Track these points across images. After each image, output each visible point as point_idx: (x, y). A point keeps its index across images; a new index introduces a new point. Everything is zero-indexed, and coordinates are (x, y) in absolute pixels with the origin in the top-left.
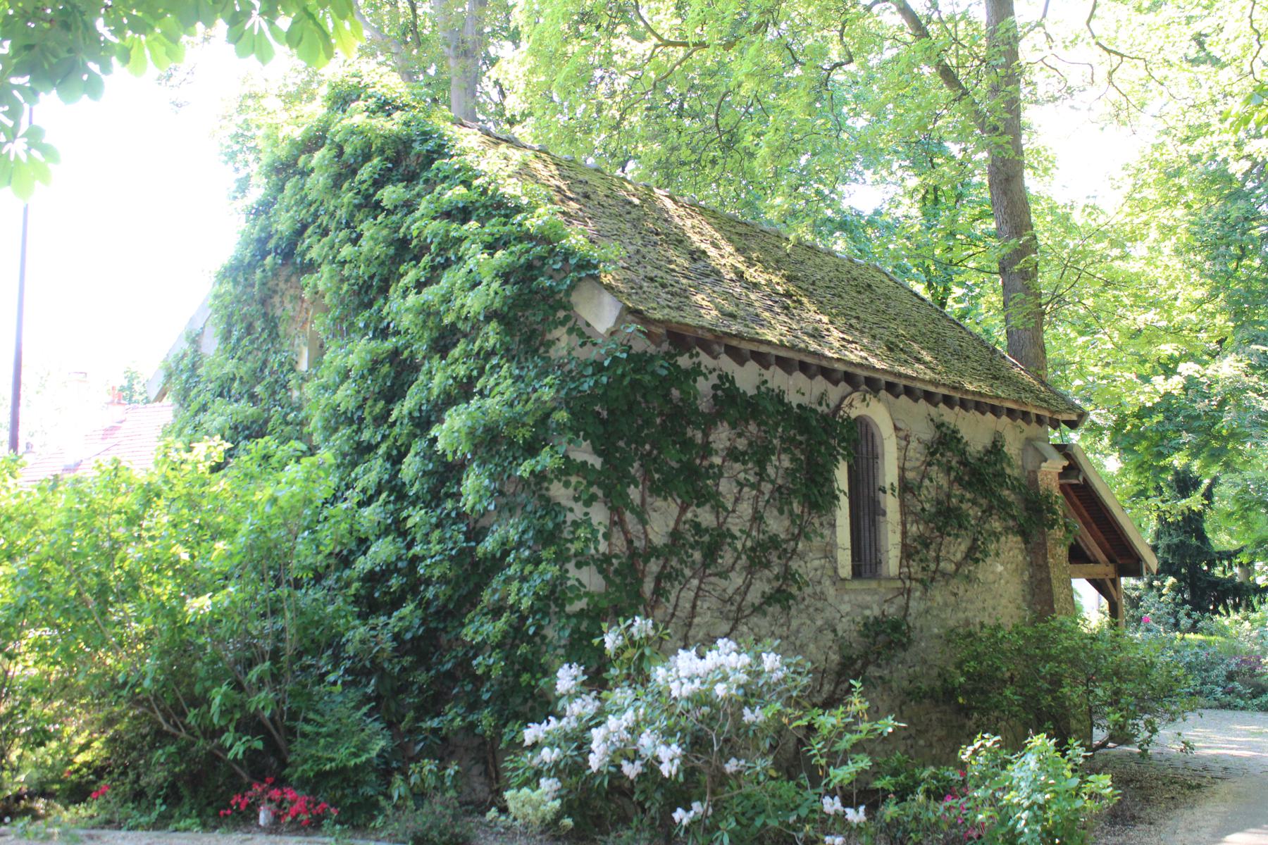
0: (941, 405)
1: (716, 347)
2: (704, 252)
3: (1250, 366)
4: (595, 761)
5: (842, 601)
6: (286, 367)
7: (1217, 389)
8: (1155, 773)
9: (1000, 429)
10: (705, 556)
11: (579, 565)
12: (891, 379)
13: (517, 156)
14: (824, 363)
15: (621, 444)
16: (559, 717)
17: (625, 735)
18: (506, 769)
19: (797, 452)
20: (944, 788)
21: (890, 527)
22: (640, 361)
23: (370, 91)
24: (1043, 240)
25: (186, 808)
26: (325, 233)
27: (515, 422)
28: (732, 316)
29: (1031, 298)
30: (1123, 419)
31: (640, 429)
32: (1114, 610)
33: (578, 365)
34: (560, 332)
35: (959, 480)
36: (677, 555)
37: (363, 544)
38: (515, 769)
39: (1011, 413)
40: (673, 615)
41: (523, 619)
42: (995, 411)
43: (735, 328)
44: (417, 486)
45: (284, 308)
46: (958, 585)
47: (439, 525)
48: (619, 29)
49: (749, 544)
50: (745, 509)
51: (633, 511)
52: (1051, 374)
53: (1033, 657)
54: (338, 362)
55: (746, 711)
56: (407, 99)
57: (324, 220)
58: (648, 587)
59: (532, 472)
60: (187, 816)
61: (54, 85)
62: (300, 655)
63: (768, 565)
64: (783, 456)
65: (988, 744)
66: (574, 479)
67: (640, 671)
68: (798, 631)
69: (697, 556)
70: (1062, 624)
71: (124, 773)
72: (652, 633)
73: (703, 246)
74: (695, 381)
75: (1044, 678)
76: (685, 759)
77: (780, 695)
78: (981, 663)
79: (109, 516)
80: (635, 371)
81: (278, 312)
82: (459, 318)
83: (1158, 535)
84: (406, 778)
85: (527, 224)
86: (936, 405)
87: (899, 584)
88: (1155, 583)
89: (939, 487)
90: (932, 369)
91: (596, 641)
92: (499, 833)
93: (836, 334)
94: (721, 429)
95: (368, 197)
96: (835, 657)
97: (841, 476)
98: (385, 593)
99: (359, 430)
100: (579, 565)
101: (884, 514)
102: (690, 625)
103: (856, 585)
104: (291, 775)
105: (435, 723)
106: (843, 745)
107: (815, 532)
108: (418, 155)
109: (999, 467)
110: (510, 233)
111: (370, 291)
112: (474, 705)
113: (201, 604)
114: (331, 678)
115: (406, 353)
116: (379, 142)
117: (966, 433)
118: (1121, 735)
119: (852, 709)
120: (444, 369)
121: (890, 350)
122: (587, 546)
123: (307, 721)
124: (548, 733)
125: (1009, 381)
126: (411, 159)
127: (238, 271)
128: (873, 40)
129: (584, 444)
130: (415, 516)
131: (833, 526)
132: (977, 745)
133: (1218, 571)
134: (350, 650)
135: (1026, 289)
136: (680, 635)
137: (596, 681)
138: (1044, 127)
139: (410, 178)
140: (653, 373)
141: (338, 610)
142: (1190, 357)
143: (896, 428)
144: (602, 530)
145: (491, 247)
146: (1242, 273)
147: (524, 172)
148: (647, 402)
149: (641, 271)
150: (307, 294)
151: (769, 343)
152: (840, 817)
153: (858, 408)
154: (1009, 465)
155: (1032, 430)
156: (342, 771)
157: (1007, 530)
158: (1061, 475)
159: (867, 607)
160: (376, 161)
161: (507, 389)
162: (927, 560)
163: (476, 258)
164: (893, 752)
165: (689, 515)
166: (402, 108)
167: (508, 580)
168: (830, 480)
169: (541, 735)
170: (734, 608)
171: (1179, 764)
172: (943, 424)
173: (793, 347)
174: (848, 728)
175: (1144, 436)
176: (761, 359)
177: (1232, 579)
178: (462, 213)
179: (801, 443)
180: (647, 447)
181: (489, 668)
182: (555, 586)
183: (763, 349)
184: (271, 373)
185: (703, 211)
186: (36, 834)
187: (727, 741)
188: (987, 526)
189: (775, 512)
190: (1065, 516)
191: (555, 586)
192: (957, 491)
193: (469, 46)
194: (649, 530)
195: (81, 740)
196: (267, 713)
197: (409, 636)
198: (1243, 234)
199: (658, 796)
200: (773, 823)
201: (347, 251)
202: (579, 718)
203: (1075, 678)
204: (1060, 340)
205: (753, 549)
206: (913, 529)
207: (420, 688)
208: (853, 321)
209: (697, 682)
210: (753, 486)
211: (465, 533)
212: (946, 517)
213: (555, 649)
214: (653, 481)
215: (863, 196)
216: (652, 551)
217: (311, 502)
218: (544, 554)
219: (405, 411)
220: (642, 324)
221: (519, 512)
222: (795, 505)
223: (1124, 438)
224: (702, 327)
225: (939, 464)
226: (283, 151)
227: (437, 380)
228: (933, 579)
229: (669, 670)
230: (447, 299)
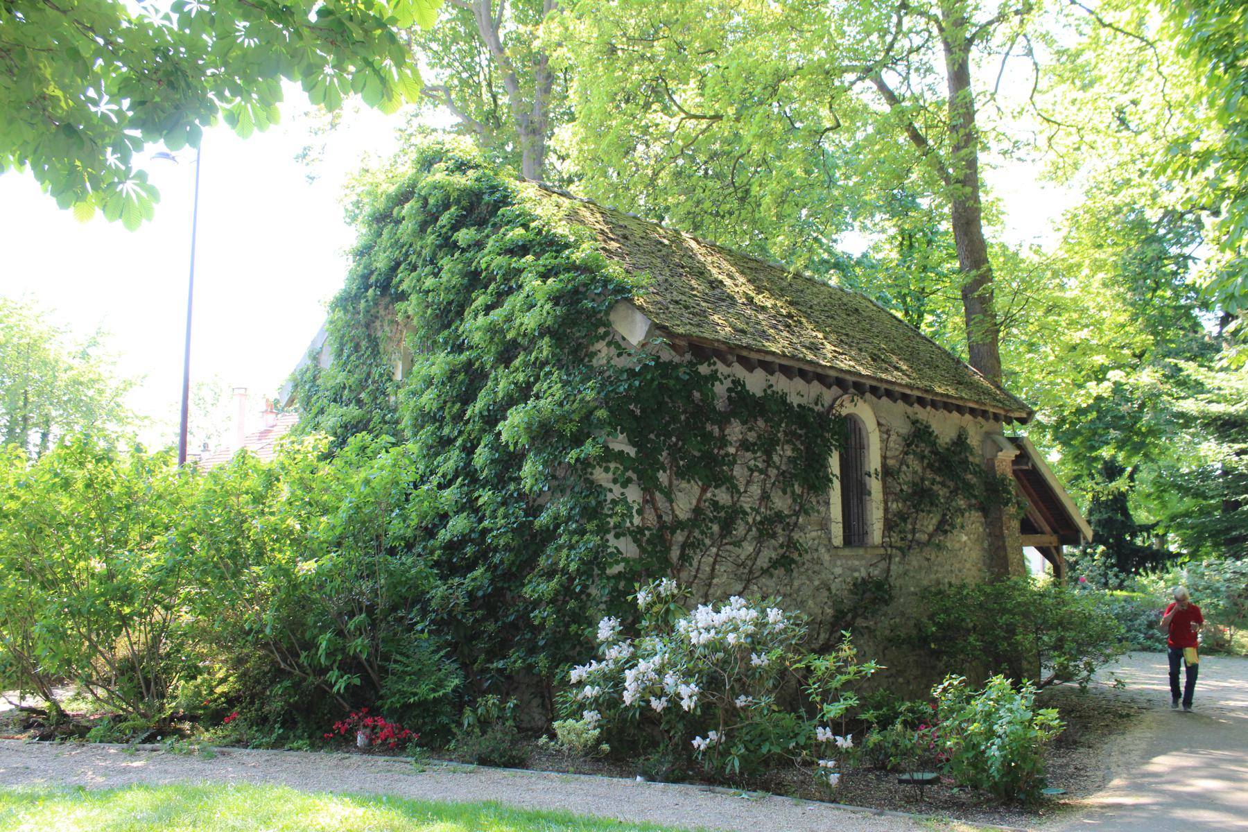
0: (916, 405)
1: (730, 357)
2: (721, 282)
3: (1164, 375)
4: (628, 697)
5: (835, 566)
6: (386, 377)
7: (1137, 394)
8: (1092, 704)
9: (963, 424)
10: (722, 528)
11: (617, 536)
12: (874, 383)
13: (566, 203)
14: (819, 370)
15: (652, 436)
16: (600, 660)
17: (653, 675)
18: (557, 702)
19: (798, 443)
20: (918, 719)
21: (874, 505)
22: (665, 368)
23: (450, 155)
24: (997, 275)
25: (299, 732)
26: (414, 268)
27: (565, 418)
28: (743, 332)
29: (988, 319)
30: (1063, 420)
31: (668, 424)
32: (1057, 572)
33: (615, 372)
34: (601, 345)
35: (930, 466)
36: (699, 527)
37: (444, 517)
38: (564, 702)
39: (972, 411)
40: (696, 577)
41: (571, 579)
42: (960, 410)
43: (745, 341)
44: (486, 472)
45: (383, 331)
46: (930, 553)
47: (504, 503)
48: (654, 107)
49: (758, 518)
50: (755, 490)
51: (661, 491)
52: (1006, 384)
53: (991, 610)
54: (424, 372)
55: (754, 656)
56: (479, 160)
57: (413, 258)
58: (675, 554)
59: (577, 460)
60: (301, 738)
61: (161, 135)
62: (394, 609)
63: (774, 536)
64: (786, 447)
65: (955, 683)
66: (612, 465)
67: (667, 623)
68: (799, 590)
69: (716, 528)
70: (1016, 583)
71: (252, 703)
72: (676, 592)
73: (720, 277)
74: (713, 385)
75: (1000, 627)
76: (702, 695)
77: (781, 642)
78: (949, 615)
79: (238, 496)
80: (662, 376)
81: (379, 334)
82: (518, 334)
83: (1091, 512)
84: (475, 711)
85: (574, 257)
86: (911, 405)
87: (882, 551)
88: (1089, 550)
89: (915, 472)
90: (908, 376)
91: (630, 598)
92: (551, 755)
93: (829, 347)
94: (974, 571)
95: (447, 239)
96: (829, 611)
97: (834, 463)
98: (462, 559)
99: (441, 427)
100: (617, 536)
101: (870, 493)
102: (710, 585)
103: (847, 552)
104: (382, 706)
105: (500, 664)
106: (835, 684)
107: (812, 508)
108: (488, 204)
109: (963, 456)
110: (559, 265)
111: (448, 314)
112: (533, 650)
113: (308, 567)
114: (419, 627)
115: (477, 364)
116: (456, 194)
117: (936, 427)
118: (1064, 674)
119: (842, 654)
120: (507, 377)
121: (874, 360)
122: (624, 520)
123: (396, 662)
124: (590, 674)
125: (972, 386)
126: (481, 207)
127: (346, 302)
128: (856, 113)
129: (621, 437)
130: (485, 496)
131: (828, 503)
132: (946, 684)
133: (1139, 541)
134: (434, 605)
135: (984, 312)
136: (702, 592)
137: (630, 631)
138: (1000, 181)
139: (481, 224)
140: (678, 378)
141: (421, 572)
142: (1120, 367)
143: (879, 424)
144: (636, 507)
145: (544, 276)
146: (1156, 301)
147: (572, 216)
148: (673, 402)
149: (668, 296)
150: (399, 318)
151: (774, 353)
152: (831, 745)
153: (847, 408)
154: (972, 454)
155: (989, 425)
156: (423, 704)
157: (970, 507)
158: (1014, 462)
159: (856, 570)
160: (453, 209)
161: (558, 391)
162: (905, 532)
163: (531, 283)
164: (877, 688)
165: (709, 495)
166: (477, 167)
167: (559, 548)
168: (824, 466)
169: (585, 675)
170: (746, 571)
171: (1111, 697)
172: (917, 421)
173: (793, 357)
174: (839, 670)
175: (1081, 433)
176: (768, 367)
177: (1150, 547)
178: (521, 249)
179: (801, 436)
180: (674, 439)
181: (544, 619)
182: (597, 553)
183: (769, 358)
184: (373, 382)
185: (721, 250)
186: (181, 751)
187: (739, 680)
188: (954, 504)
189: (780, 493)
190: (1017, 496)
191: (597, 553)
192: (929, 475)
193: (537, 125)
194: (676, 507)
195: (221, 675)
196: (364, 656)
197: (480, 593)
198: (1157, 270)
199: (680, 726)
200: (777, 750)
201: (430, 282)
202: (616, 662)
203: (1026, 627)
204: (1012, 355)
205: (761, 523)
206: (894, 506)
207: (490, 636)
208: (843, 338)
209: (713, 632)
210: (761, 472)
211: (524, 510)
212: (920, 497)
213: (598, 604)
214: (679, 468)
215: (851, 242)
216: (678, 525)
217: (398, 484)
218: (589, 527)
219: (477, 411)
220: (667, 337)
221: (568, 492)
222: (796, 487)
223: (1064, 433)
224: (718, 340)
225: (915, 453)
226: (381, 205)
227: (501, 386)
228: (910, 547)
229: (690, 622)
230: (509, 319)
